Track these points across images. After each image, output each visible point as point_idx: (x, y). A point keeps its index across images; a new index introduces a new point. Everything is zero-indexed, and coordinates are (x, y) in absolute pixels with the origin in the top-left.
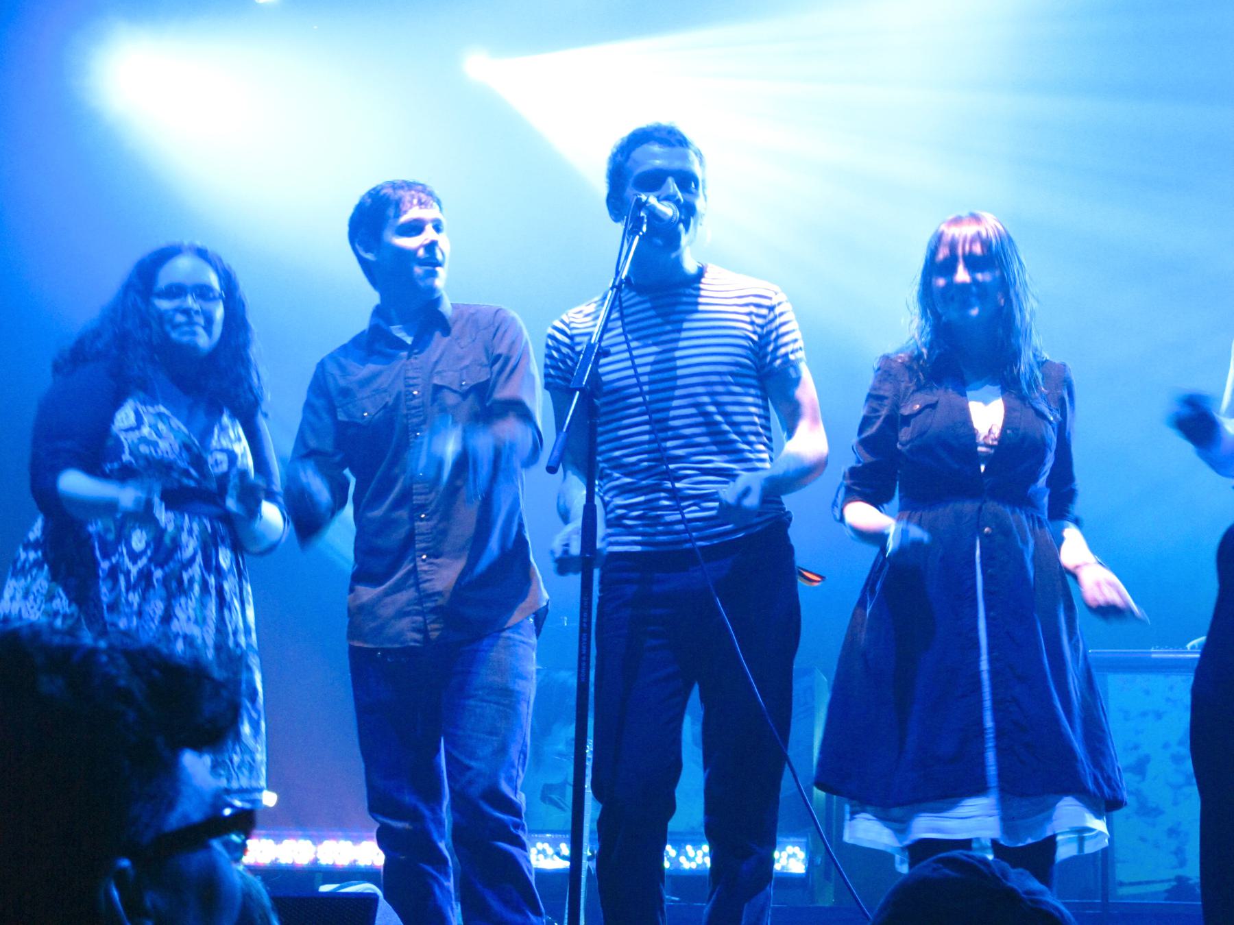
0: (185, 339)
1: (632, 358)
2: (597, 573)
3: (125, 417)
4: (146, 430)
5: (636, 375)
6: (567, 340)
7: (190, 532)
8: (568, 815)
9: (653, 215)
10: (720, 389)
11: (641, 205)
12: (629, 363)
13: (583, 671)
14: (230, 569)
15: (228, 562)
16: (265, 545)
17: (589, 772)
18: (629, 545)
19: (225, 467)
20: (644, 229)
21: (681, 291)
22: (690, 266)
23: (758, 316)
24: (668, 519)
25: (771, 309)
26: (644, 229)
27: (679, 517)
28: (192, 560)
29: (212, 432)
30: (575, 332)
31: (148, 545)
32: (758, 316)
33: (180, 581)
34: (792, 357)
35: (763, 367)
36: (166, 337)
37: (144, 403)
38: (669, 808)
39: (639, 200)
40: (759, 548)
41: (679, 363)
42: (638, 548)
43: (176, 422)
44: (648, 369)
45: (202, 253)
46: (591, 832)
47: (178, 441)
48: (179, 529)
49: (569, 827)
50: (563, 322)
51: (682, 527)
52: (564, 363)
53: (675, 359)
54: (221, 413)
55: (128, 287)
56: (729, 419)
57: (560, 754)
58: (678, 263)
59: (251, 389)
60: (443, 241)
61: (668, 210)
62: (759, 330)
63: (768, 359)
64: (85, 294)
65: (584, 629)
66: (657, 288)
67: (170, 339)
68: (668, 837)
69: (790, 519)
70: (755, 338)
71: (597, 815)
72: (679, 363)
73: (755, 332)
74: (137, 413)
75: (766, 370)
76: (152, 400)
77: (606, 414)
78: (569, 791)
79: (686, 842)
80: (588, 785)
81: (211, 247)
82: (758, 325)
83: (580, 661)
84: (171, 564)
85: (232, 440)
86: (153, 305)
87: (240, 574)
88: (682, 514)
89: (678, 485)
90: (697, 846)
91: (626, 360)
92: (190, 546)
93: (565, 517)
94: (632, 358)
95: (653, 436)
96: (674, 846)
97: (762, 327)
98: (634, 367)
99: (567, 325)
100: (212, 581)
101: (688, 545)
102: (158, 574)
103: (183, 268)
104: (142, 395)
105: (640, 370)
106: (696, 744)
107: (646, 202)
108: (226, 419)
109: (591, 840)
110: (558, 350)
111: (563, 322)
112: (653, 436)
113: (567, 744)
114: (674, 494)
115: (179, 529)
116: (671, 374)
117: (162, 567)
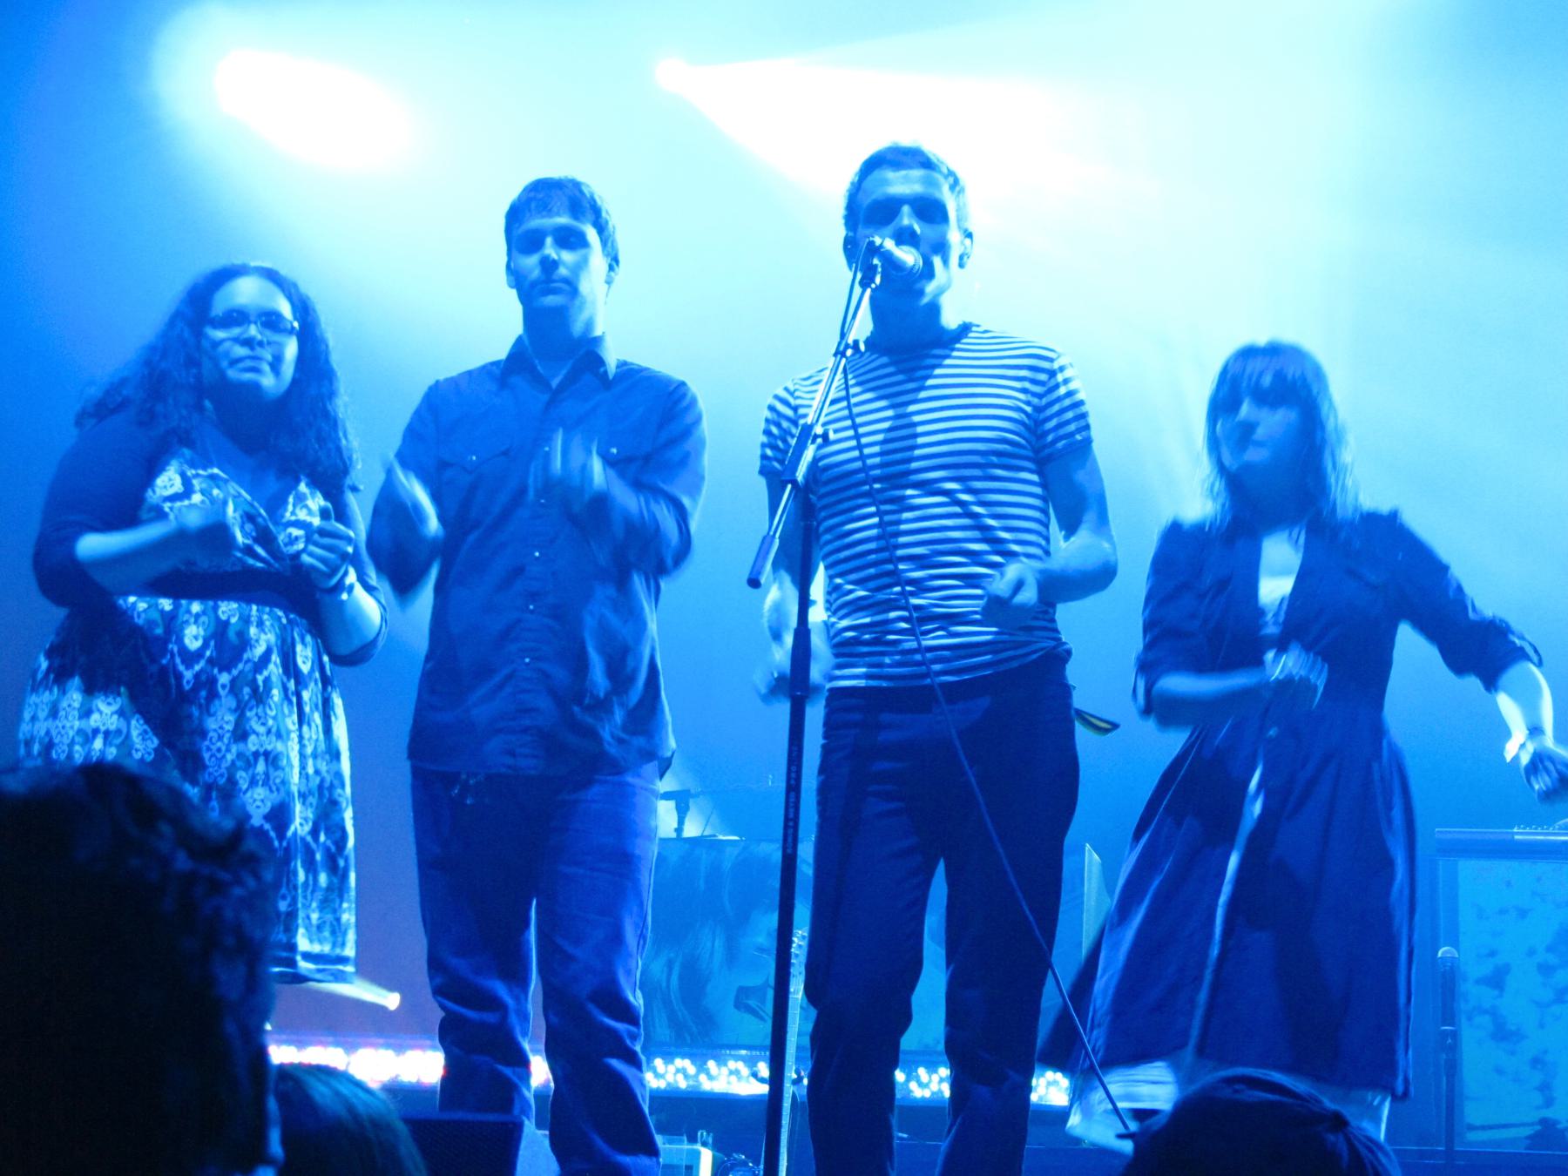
0: (248, 376)
1: (857, 437)
3: (168, 481)
5: (862, 457)
6: (789, 413)
7: (260, 624)
8: (767, 1027)
9: (890, 262)
11: (874, 250)
12: (853, 443)
13: (790, 840)
14: (312, 671)
15: (309, 664)
16: (356, 643)
18: (854, 677)
20: (878, 280)
22: (950, 319)
23: (1033, 381)
25: (1052, 374)
26: (878, 280)
28: (265, 659)
29: (285, 502)
32: (1033, 381)
33: (255, 689)
36: (223, 375)
37: (193, 465)
38: (903, 1018)
39: (871, 243)
40: (1022, 689)
41: (920, 429)
42: (862, 683)
43: (233, 487)
44: (876, 449)
45: (271, 276)
46: (799, 1048)
47: (240, 512)
48: (246, 620)
49: (768, 1042)
50: (786, 389)
51: (918, 657)
52: (785, 441)
53: (915, 425)
54: (298, 481)
55: (176, 316)
57: (762, 950)
59: (339, 449)
61: (908, 256)
63: (1050, 438)
64: (120, 327)
66: (905, 339)
67: (230, 384)
68: (901, 1057)
70: (1028, 409)
71: (809, 1027)
72: (920, 429)
73: (1028, 403)
74: (183, 475)
75: (1047, 451)
77: (824, 507)
78: (770, 994)
79: (918, 1064)
81: (283, 272)
82: (1034, 394)
83: (786, 827)
84: (240, 666)
85: (309, 506)
86: (207, 337)
87: (326, 681)
88: (918, 640)
90: (932, 1067)
91: (857, 404)
94: (857, 437)
95: (882, 543)
96: (903, 1070)
97: (1040, 396)
99: (792, 394)
100: (292, 685)
101: (928, 681)
102: (224, 678)
103: (246, 292)
104: (187, 452)
105: (867, 451)
107: (881, 246)
108: (303, 487)
109: (798, 1059)
110: (778, 425)
111: (786, 389)
113: (769, 934)
114: (923, 618)
115: (246, 620)
116: (909, 442)
117: (228, 670)
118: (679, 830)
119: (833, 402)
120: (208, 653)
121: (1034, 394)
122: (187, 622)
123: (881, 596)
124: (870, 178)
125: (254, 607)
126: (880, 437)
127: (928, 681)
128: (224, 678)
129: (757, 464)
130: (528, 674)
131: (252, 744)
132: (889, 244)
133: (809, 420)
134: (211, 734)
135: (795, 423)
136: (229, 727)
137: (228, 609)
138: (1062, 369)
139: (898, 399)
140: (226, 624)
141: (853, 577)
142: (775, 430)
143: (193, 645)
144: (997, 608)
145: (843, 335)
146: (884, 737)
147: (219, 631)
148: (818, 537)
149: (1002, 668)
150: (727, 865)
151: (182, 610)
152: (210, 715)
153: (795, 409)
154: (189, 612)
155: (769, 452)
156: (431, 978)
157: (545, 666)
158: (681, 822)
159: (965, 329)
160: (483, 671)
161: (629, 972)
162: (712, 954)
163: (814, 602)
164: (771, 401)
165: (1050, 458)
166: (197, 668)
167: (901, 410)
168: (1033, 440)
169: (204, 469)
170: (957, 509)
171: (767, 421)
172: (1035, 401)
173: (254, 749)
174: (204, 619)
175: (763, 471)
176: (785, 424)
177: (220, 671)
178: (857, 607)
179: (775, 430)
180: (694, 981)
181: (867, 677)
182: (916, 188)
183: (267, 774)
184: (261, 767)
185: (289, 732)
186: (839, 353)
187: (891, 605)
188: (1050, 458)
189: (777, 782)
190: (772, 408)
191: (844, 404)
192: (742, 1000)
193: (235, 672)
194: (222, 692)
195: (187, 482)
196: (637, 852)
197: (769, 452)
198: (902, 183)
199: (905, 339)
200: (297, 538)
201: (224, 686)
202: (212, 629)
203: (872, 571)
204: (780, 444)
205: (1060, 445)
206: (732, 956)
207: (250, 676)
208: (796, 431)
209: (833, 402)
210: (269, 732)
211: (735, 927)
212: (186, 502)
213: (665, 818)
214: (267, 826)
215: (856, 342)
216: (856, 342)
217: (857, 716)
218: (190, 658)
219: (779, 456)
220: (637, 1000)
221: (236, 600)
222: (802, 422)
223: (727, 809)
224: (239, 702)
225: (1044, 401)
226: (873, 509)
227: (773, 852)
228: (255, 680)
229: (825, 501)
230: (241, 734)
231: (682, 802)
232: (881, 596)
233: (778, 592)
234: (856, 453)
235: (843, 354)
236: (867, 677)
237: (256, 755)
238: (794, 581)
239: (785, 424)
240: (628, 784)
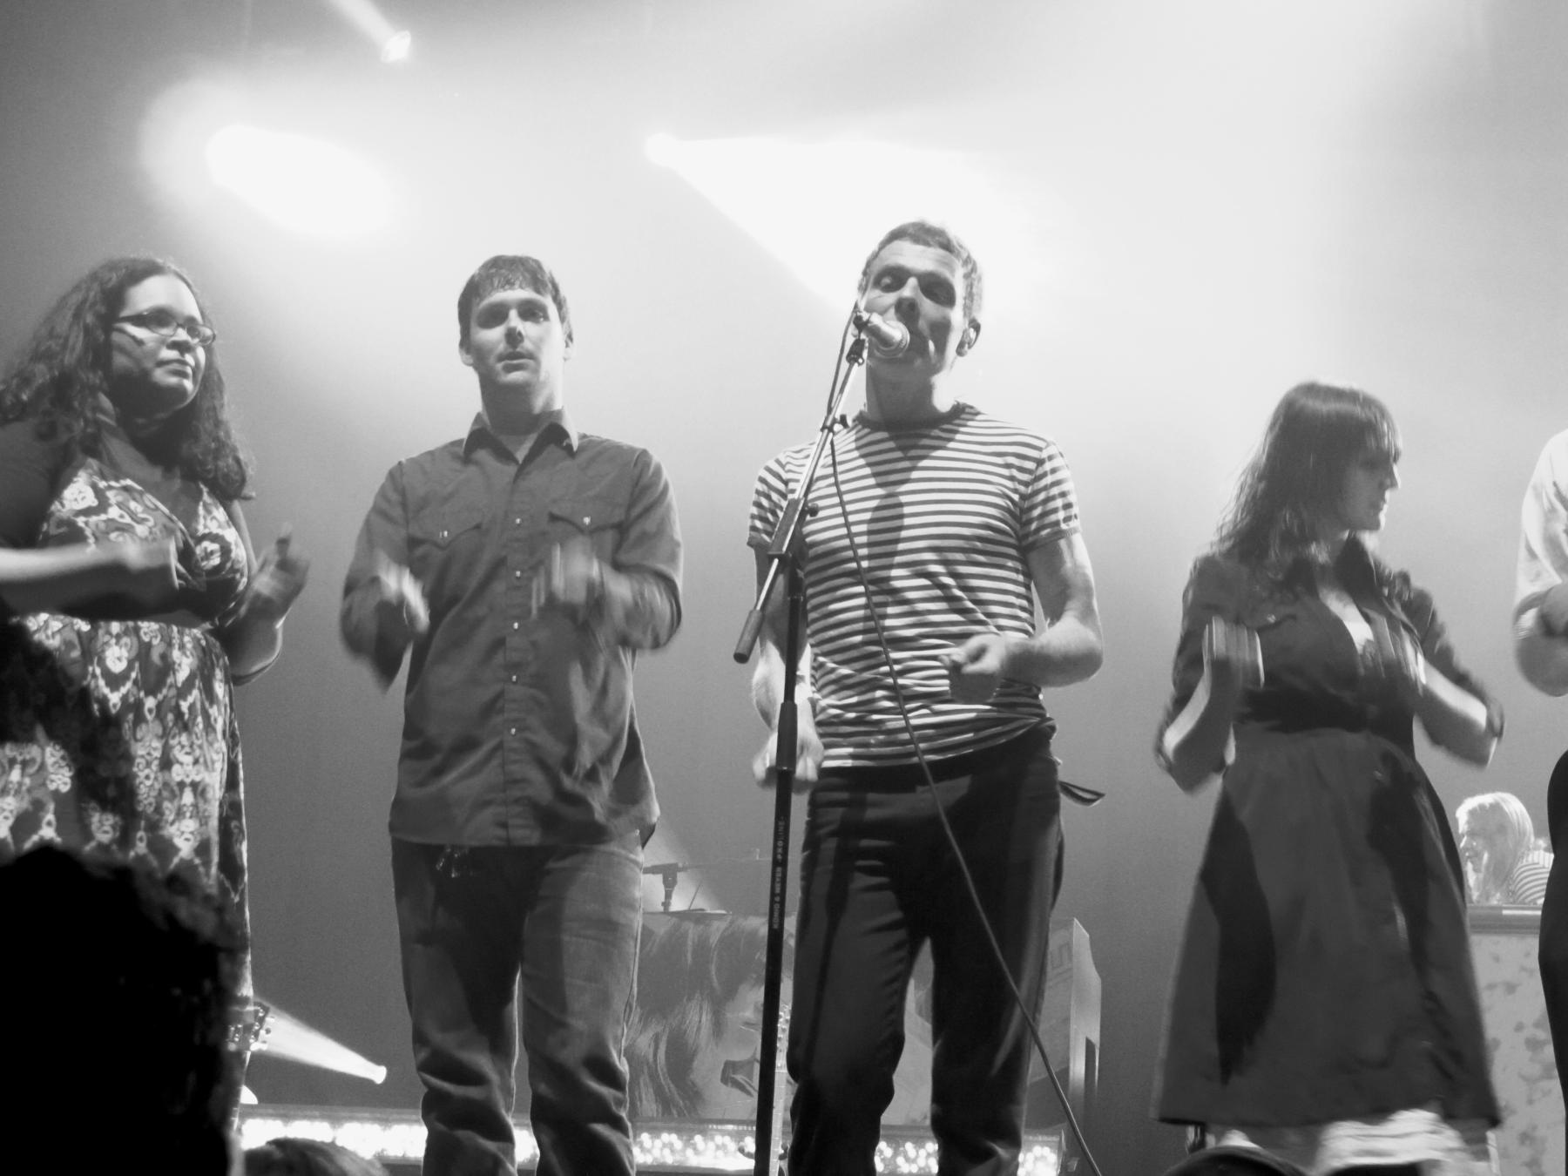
0: (173, 380)
4: (114, 512)
5: (850, 535)
6: (781, 486)
7: (182, 647)
10: (959, 556)
13: (776, 914)
17: (783, 1045)
18: (841, 757)
19: (216, 561)
21: (926, 432)
22: (943, 401)
23: (1021, 469)
24: (891, 725)
25: (1040, 462)
27: (903, 723)
31: (130, 668)
32: (1021, 469)
34: (1063, 526)
35: (1027, 536)
37: (103, 477)
41: (906, 510)
42: (849, 763)
43: (150, 499)
44: (864, 528)
50: (778, 462)
51: (906, 736)
52: (774, 514)
53: (901, 505)
56: (973, 596)
57: (747, 1024)
58: (927, 390)
60: (1072, 498)
62: (1022, 488)
63: (1034, 526)
65: (780, 863)
66: (904, 420)
70: (1016, 497)
73: (1015, 491)
75: (1031, 539)
76: (113, 470)
77: (813, 585)
78: (757, 1067)
80: (781, 1062)
82: (1021, 482)
83: (772, 902)
84: (165, 691)
88: (906, 719)
89: (901, 681)
91: (842, 463)
92: (185, 665)
93: (766, 716)
94: (845, 514)
97: (1026, 484)
98: (847, 525)
99: (783, 466)
101: (915, 759)
102: (150, 703)
105: (854, 529)
106: (920, 1013)
110: (768, 497)
111: (778, 462)
112: (868, 612)
114: (898, 694)
118: (666, 904)
120: (133, 675)
121: (1021, 482)
122: (107, 643)
123: (867, 675)
125: (175, 629)
126: (868, 516)
127: (915, 759)
128: (150, 703)
130: (516, 745)
131: (177, 773)
133: (795, 496)
134: (138, 760)
135: (784, 496)
136: (157, 754)
137: (149, 628)
138: (1050, 458)
139: (886, 476)
140: (149, 646)
141: (839, 657)
142: (765, 502)
143: (117, 667)
144: (964, 684)
145: (830, 410)
146: (871, 814)
147: (144, 651)
148: (806, 613)
149: (983, 746)
150: (714, 940)
151: (101, 632)
152: (136, 740)
153: (786, 483)
154: (109, 633)
155: (759, 524)
156: (416, 1052)
157: (528, 735)
158: (668, 896)
159: (960, 412)
160: (466, 745)
161: (617, 1041)
162: (699, 1029)
163: (802, 678)
165: (1032, 547)
166: (123, 690)
167: (891, 489)
168: (1018, 526)
169: (117, 480)
170: (938, 592)
171: (753, 517)
172: (1022, 488)
173: (178, 779)
174: (125, 640)
176: (775, 497)
177: (147, 694)
178: (841, 685)
179: (765, 502)
180: (681, 1057)
181: (853, 757)
183: (195, 806)
184: (188, 798)
185: (213, 762)
187: (873, 685)
188: (1032, 547)
189: (763, 857)
190: (762, 480)
191: (832, 480)
192: (729, 1073)
193: (160, 697)
194: (149, 717)
195: (99, 493)
196: (622, 921)
197: (759, 524)
199: (904, 420)
200: (212, 553)
201: (150, 711)
202: (134, 653)
204: (770, 516)
205: (1044, 533)
206: (718, 1028)
207: (173, 703)
208: (784, 504)
210: (196, 762)
211: (720, 1003)
212: (103, 517)
213: (649, 890)
214: (197, 861)
217: (844, 796)
218: (115, 681)
219: (769, 528)
220: (623, 1066)
221: (156, 621)
222: (790, 496)
223: (714, 880)
224: (164, 728)
225: (1030, 490)
226: (861, 589)
227: (759, 925)
228: (178, 706)
229: (813, 578)
230: (166, 763)
231: (669, 875)
232: (867, 675)
233: (769, 666)
234: (844, 531)
235: (831, 429)
236: (853, 757)
237: (182, 785)
238: (782, 655)
239: (775, 497)
240: (613, 854)
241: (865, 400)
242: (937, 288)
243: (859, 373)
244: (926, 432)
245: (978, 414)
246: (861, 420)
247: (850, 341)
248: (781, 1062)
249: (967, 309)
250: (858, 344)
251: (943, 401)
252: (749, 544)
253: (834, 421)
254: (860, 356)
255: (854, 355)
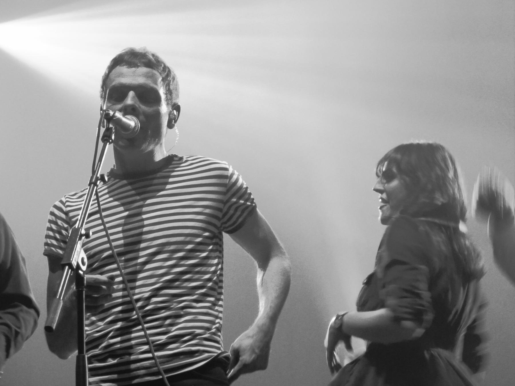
2: (58, 297)
6: (63, 216)
12: (102, 227)
30: (69, 209)
50: (61, 202)
52: (60, 233)
53: (143, 220)
66: (136, 166)
69: (403, 149)
91: (108, 222)
95: (126, 293)
107: (114, 116)
110: (56, 223)
111: (61, 202)
119: (92, 205)
124: (113, 71)
129: (42, 249)
132: (118, 115)
142: (54, 227)
145: (94, 172)
159: (171, 161)
164: (44, 240)
171: (50, 221)
175: (49, 254)
179: (54, 227)
182: (141, 80)
186: (93, 183)
190: (52, 214)
198: (130, 76)
199: (136, 166)
203: (120, 300)
209: (92, 205)
215: (102, 176)
216: (102, 176)
235: (95, 184)
241: (114, 161)
242: (148, 96)
243: (109, 148)
244: (154, 176)
245: (181, 158)
246: (112, 174)
247: (103, 130)
248: (59, 293)
249: (169, 100)
250: (108, 130)
251: (160, 154)
252: (45, 254)
253: (97, 179)
254: (110, 137)
255: (106, 138)
